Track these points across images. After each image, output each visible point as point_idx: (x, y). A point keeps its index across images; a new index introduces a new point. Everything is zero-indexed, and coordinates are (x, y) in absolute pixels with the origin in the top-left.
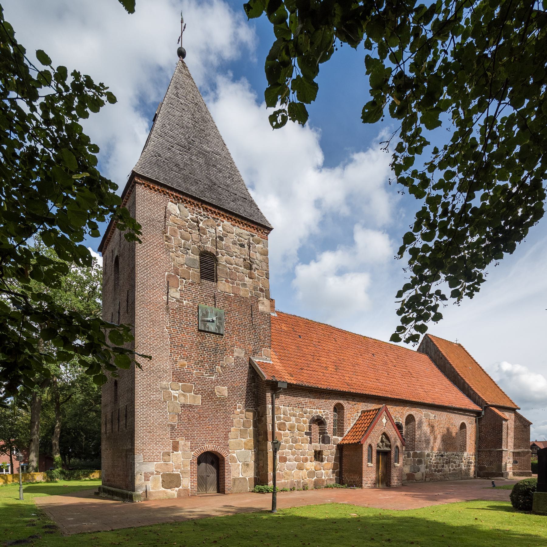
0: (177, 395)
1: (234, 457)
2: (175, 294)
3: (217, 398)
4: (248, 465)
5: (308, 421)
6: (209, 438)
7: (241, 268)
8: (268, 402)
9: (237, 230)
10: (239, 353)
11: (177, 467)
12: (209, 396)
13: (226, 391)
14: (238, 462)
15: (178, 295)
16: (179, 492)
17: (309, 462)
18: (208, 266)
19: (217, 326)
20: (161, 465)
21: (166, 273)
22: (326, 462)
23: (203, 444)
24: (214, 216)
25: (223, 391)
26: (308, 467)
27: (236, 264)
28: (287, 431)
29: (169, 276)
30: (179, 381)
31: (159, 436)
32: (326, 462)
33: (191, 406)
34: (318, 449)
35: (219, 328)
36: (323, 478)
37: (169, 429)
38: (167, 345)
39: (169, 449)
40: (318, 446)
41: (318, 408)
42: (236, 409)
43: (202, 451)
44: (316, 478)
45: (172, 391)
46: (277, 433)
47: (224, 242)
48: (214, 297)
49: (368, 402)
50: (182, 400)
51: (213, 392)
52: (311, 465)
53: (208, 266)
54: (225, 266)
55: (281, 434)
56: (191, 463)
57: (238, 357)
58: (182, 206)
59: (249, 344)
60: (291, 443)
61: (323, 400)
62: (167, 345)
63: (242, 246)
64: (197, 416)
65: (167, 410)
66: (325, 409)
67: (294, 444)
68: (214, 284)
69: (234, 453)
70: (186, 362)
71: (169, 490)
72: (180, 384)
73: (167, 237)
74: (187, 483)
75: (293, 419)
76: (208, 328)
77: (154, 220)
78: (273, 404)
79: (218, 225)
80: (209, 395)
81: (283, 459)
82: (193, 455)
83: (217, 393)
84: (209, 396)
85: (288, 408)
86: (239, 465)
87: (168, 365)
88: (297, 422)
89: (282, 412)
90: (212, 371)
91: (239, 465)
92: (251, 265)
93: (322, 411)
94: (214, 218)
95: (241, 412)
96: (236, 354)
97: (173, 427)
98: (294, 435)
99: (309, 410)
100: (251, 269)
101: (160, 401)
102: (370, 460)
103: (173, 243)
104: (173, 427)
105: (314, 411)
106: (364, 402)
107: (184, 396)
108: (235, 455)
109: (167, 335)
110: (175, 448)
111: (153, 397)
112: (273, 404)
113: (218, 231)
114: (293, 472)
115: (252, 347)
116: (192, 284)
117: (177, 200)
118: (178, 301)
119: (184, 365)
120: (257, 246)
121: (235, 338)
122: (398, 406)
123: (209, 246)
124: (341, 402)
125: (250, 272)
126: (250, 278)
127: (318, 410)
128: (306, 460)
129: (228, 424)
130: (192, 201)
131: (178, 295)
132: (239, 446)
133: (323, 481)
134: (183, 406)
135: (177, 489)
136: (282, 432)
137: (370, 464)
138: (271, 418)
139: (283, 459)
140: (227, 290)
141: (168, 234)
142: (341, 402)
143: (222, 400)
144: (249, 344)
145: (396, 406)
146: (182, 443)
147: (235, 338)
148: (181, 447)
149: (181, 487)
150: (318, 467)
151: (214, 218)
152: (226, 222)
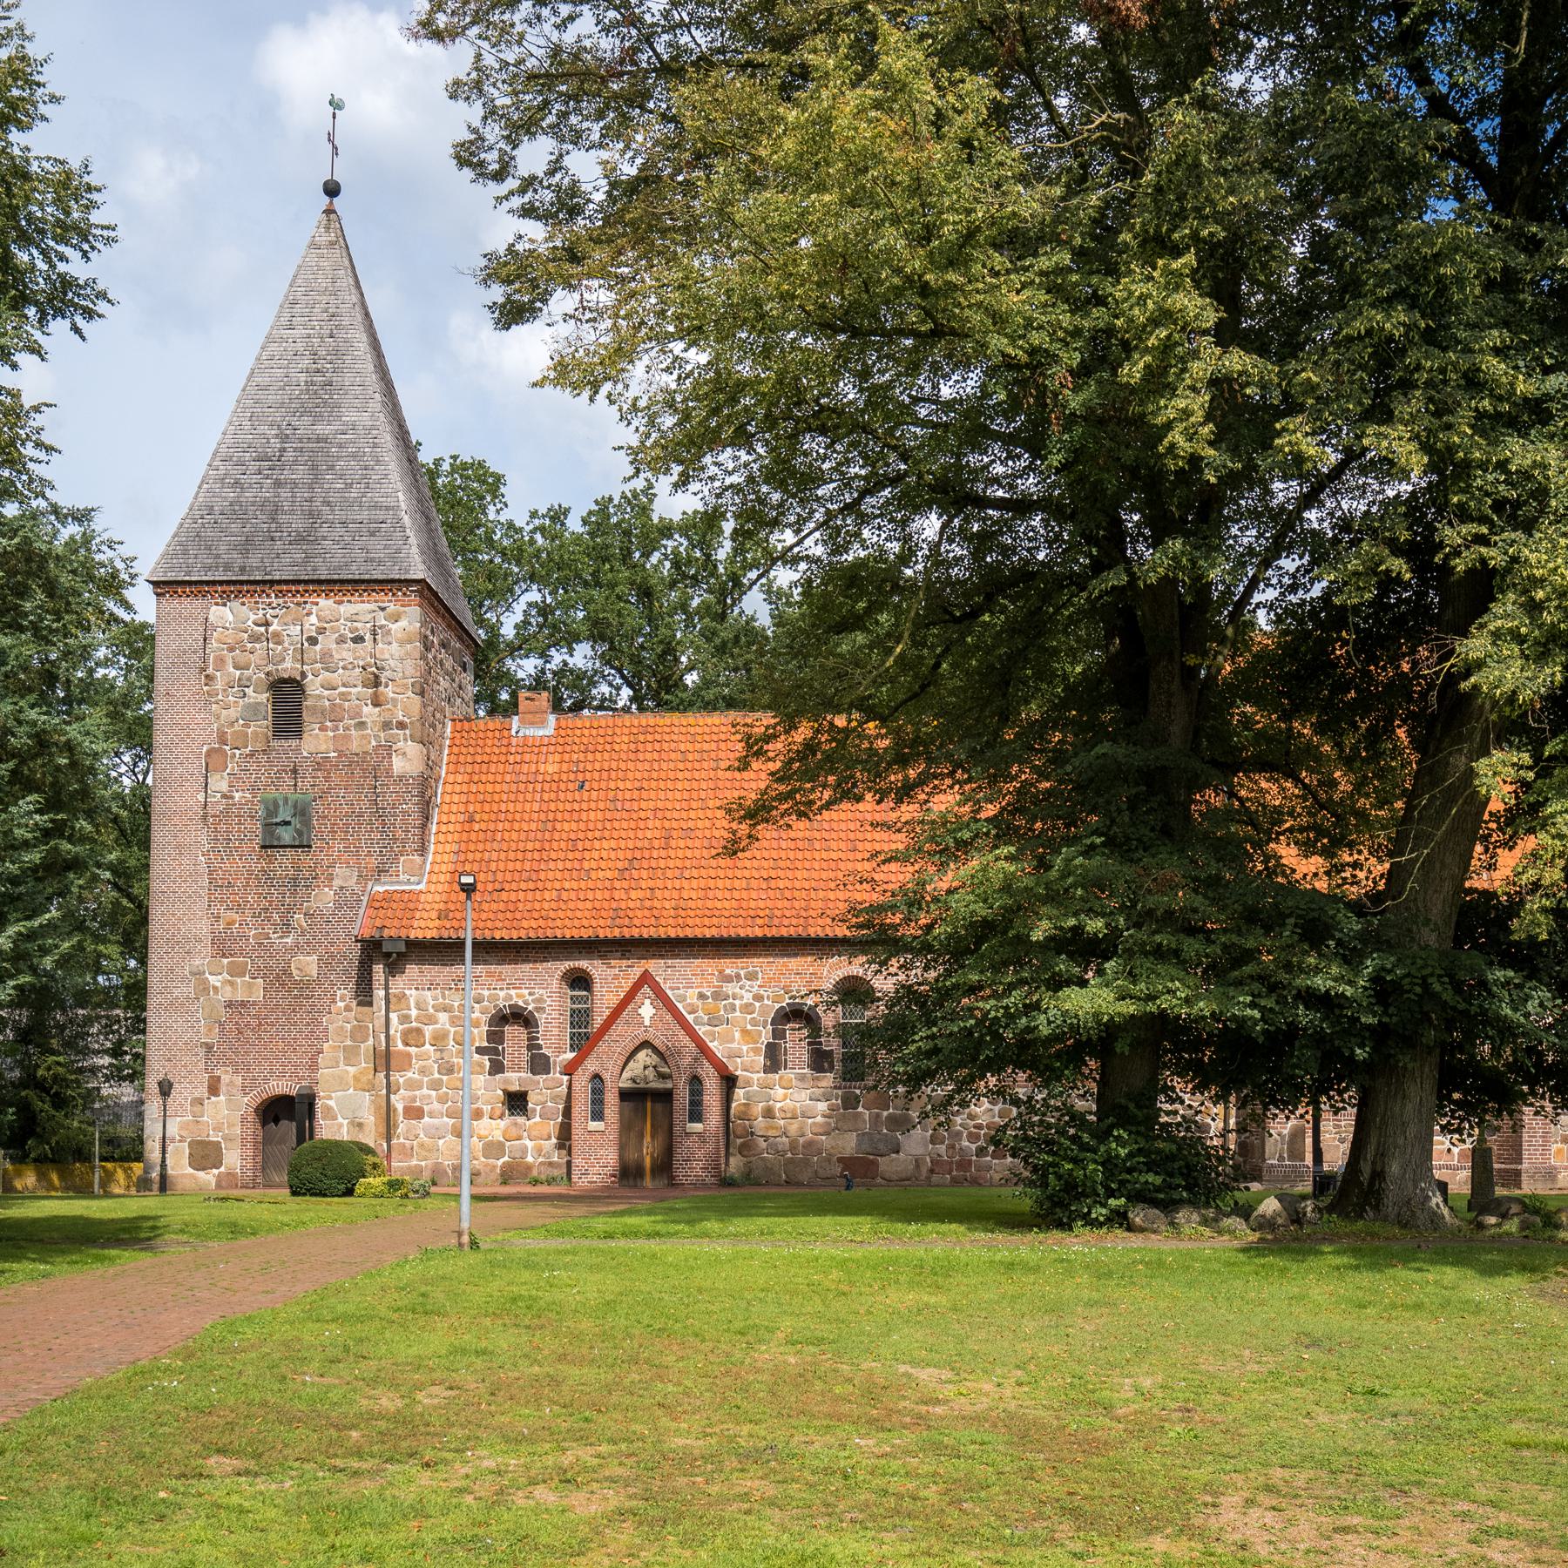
0: (218, 984)
1: (329, 1108)
2: (219, 783)
3: (296, 983)
4: (360, 1125)
5: (485, 1018)
6: (278, 1068)
7: (353, 690)
8: (376, 984)
9: (346, 609)
10: (345, 879)
11: (217, 1129)
12: (280, 979)
13: (315, 966)
14: (340, 1119)
15: (224, 786)
16: (219, 1178)
17: (486, 1120)
18: (287, 701)
19: (297, 831)
20: (187, 1123)
21: (205, 749)
22: (537, 1119)
23: (266, 1080)
24: (299, 599)
25: (307, 965)
26: (482, 1133)
27: (344, 685)
28: (427, 1046)
29: (208, 754)
30: (224, 956)
31: (185, 1066)
32: (537, 1119)
33: (243, 1004)
34: (515, 1088)
35: (300, 833)
36: (530, 1159)
37: (202, 1052)
38: (202, 888)
39: (202, 1091)
40: (515, 1079)
41: (511, 986)
42: (334, 1001)
43: (265, 1096)
44: (506, 1158)
45: (211, 978)
46: (400, 1053)
47: (318, 648)
48: (295, 771)
49: (677, 956)
50: (227, 994)
51: (286, 972)
52: (495, 1128)
53: (287, 701)
54: (320, 697)
55: (409, 1055)
56: (243, 1119)
57: (342, 888)
58: (236, 604)
59: (369, 854)
60: (437, 1075)
61: (527, 967)
62: (202, 888)
63: (359, 640)
64: (254, 1023)
65: (200, 1015)
66: (538, 988)
67: (445, 1078)
68: (294, 743)
69: (330, 1098)
70: (236, 917)
71: (201, 1174)
72: (225, 961)
73: (207, 676)
74: (235, 1159)
75: (443, 1017)
76: (279, 839)
77: (185, 652)
78: (387, 988)
79: (308, 614)
80: (278, 977)
81: (414, 1113)
82: (248, 1102)
83: (295, 972)
84: (280, 979)
85: (429, 993)
86: (341, 1125)
87: (203, 928)
88: (452, 1023)
89: (412, 1005)
90: (287, 926)
91: (341, 1125)
92: (377, 677)
93: (526, 992)
94: (298, 604)
95: (348, 1009)
96: (337, 883)
97: (209, 1047)
98: (445, 1055)
99: (486, 993)
100: (377, 684)
101: (188, 998)
102: (598, 1115)
103: (219, 685)
104: (209, 1047)
105: (502, 994)
106: (662, 957)
107: (232, 984)
108: (331, 1103)
109: (203, 868)
110: (214, 1089)
111: (176, 992)
112: (387, 988)
113: (307, 626)
114: (441, 1142)
115: (374, 861)
116: (252, 756)
117: (225, 598)
118: (224, 796)
119: (233, 922)
120: (393, 627)
121: (339, 846)
122: (796, 955)
123: (289, 667)
124: (583, 964)
125: (375, 694)
126: (376, 704)
127: (513, 992)
128: (478, 1115)
129: (317, 1034)
130: (252, 588)
131: (224, 786)
132: (342, 1084)
133: (529, 1167)
134: (229, 1005)
135: (215, 1171)
136: (413, 1050)
137: (594, 1125)
138: (383, 1019)
139: (414, 1113)
140: (323, 748)
141: (210, 671)
142: (583, 964)
143: (305, 985)
144: (369, 854)
145: (788, 956)
146: (225, 1078)
147: (339, 846)
148: (223, 1088)
149: (222, 1169)
150: (514, 1132)
151: (298, 604)
152: (322, 602)
